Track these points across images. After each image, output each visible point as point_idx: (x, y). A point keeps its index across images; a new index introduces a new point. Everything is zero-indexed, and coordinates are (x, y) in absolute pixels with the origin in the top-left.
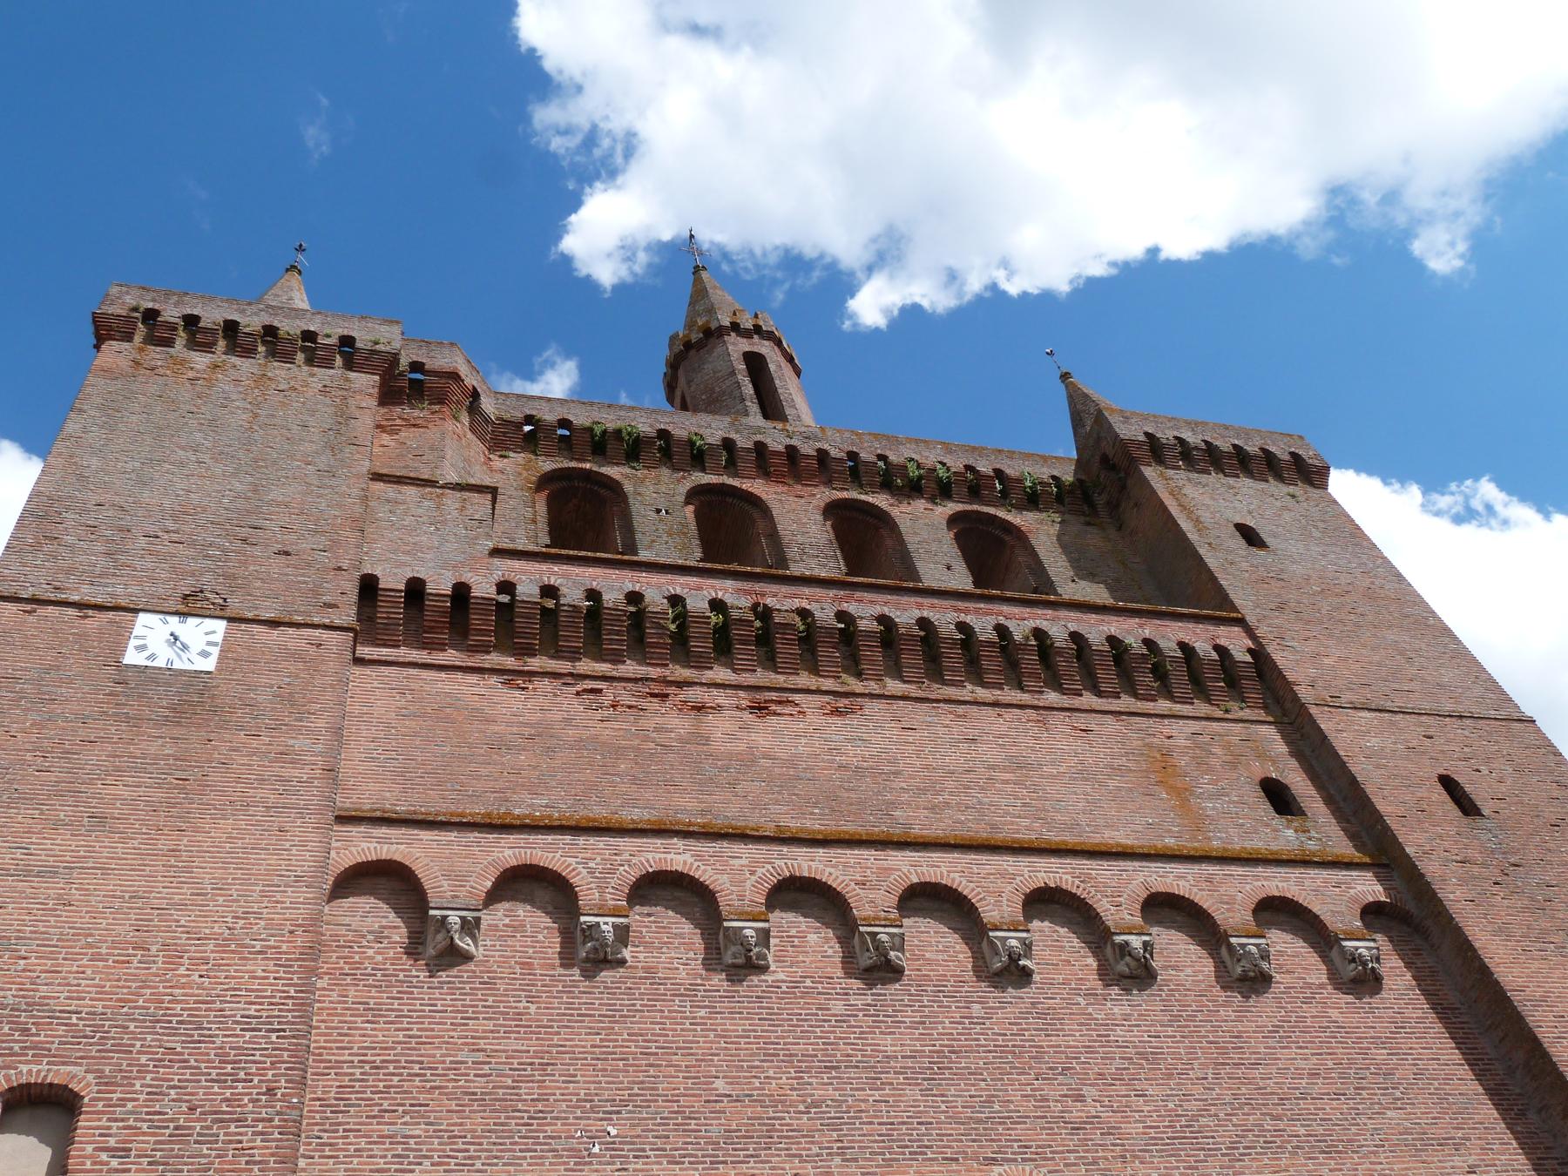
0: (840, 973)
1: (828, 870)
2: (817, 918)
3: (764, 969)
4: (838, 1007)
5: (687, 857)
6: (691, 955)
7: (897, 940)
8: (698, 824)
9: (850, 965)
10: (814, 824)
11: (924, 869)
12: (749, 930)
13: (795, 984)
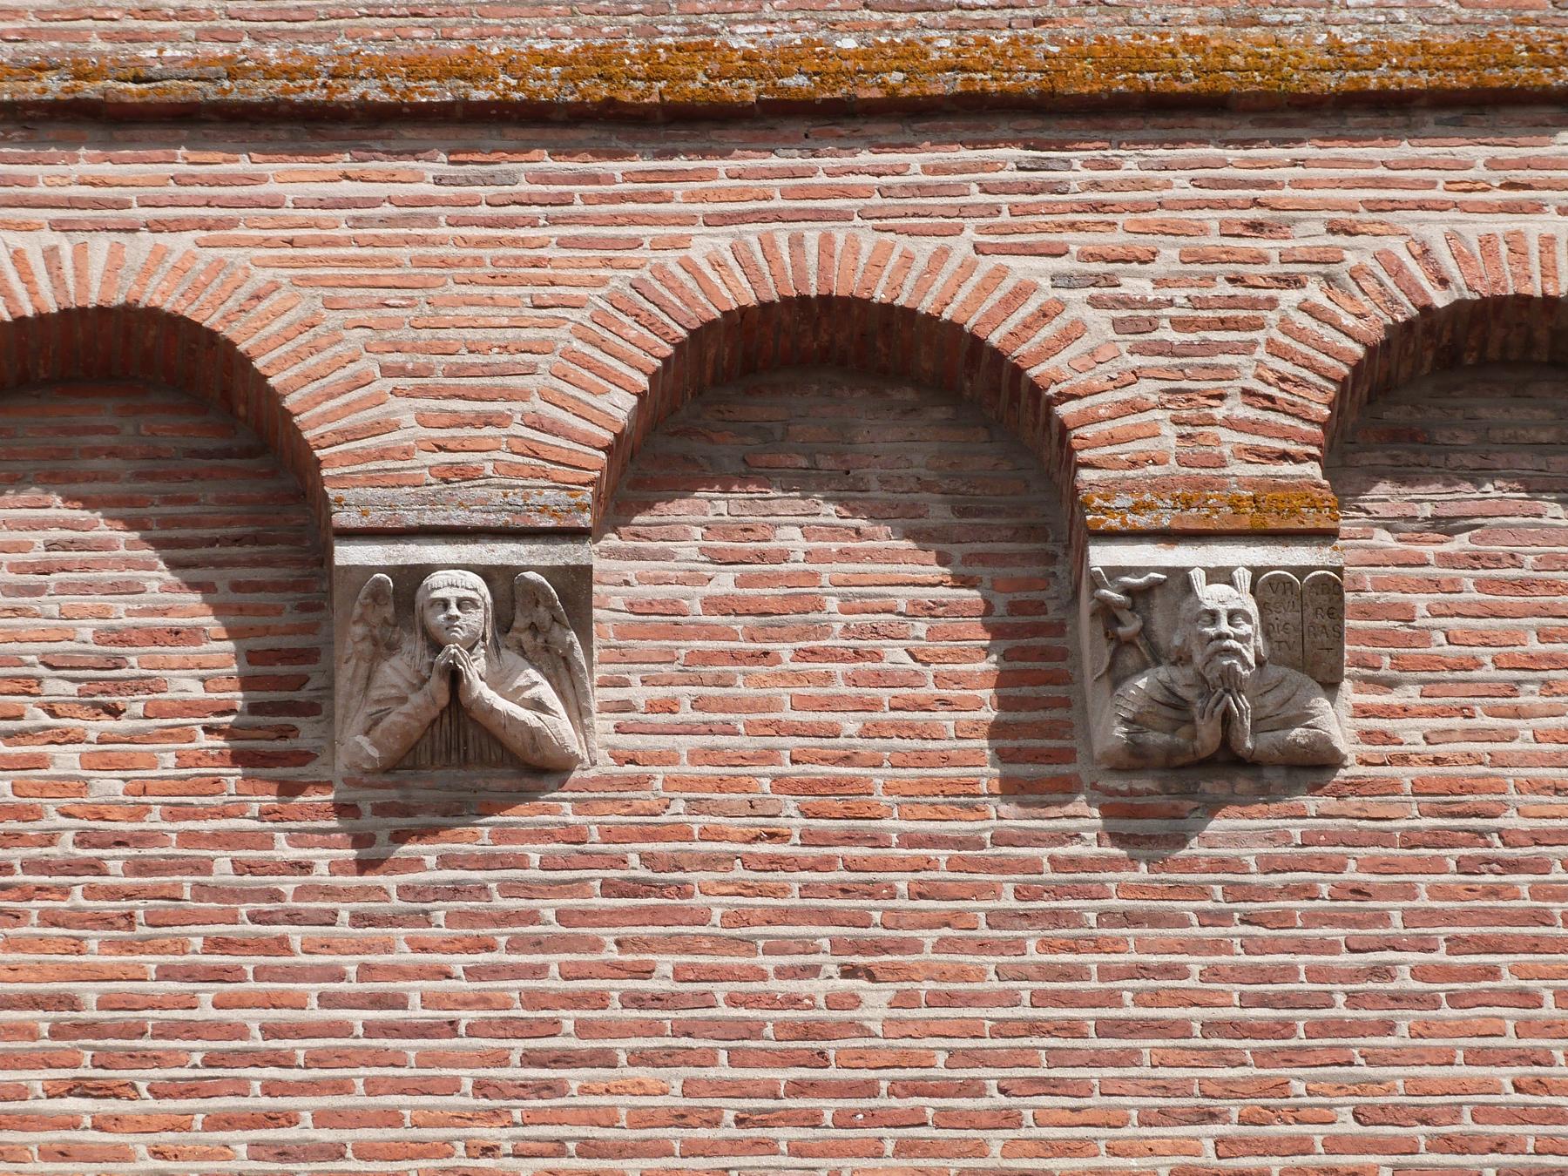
12: (1225, 582)
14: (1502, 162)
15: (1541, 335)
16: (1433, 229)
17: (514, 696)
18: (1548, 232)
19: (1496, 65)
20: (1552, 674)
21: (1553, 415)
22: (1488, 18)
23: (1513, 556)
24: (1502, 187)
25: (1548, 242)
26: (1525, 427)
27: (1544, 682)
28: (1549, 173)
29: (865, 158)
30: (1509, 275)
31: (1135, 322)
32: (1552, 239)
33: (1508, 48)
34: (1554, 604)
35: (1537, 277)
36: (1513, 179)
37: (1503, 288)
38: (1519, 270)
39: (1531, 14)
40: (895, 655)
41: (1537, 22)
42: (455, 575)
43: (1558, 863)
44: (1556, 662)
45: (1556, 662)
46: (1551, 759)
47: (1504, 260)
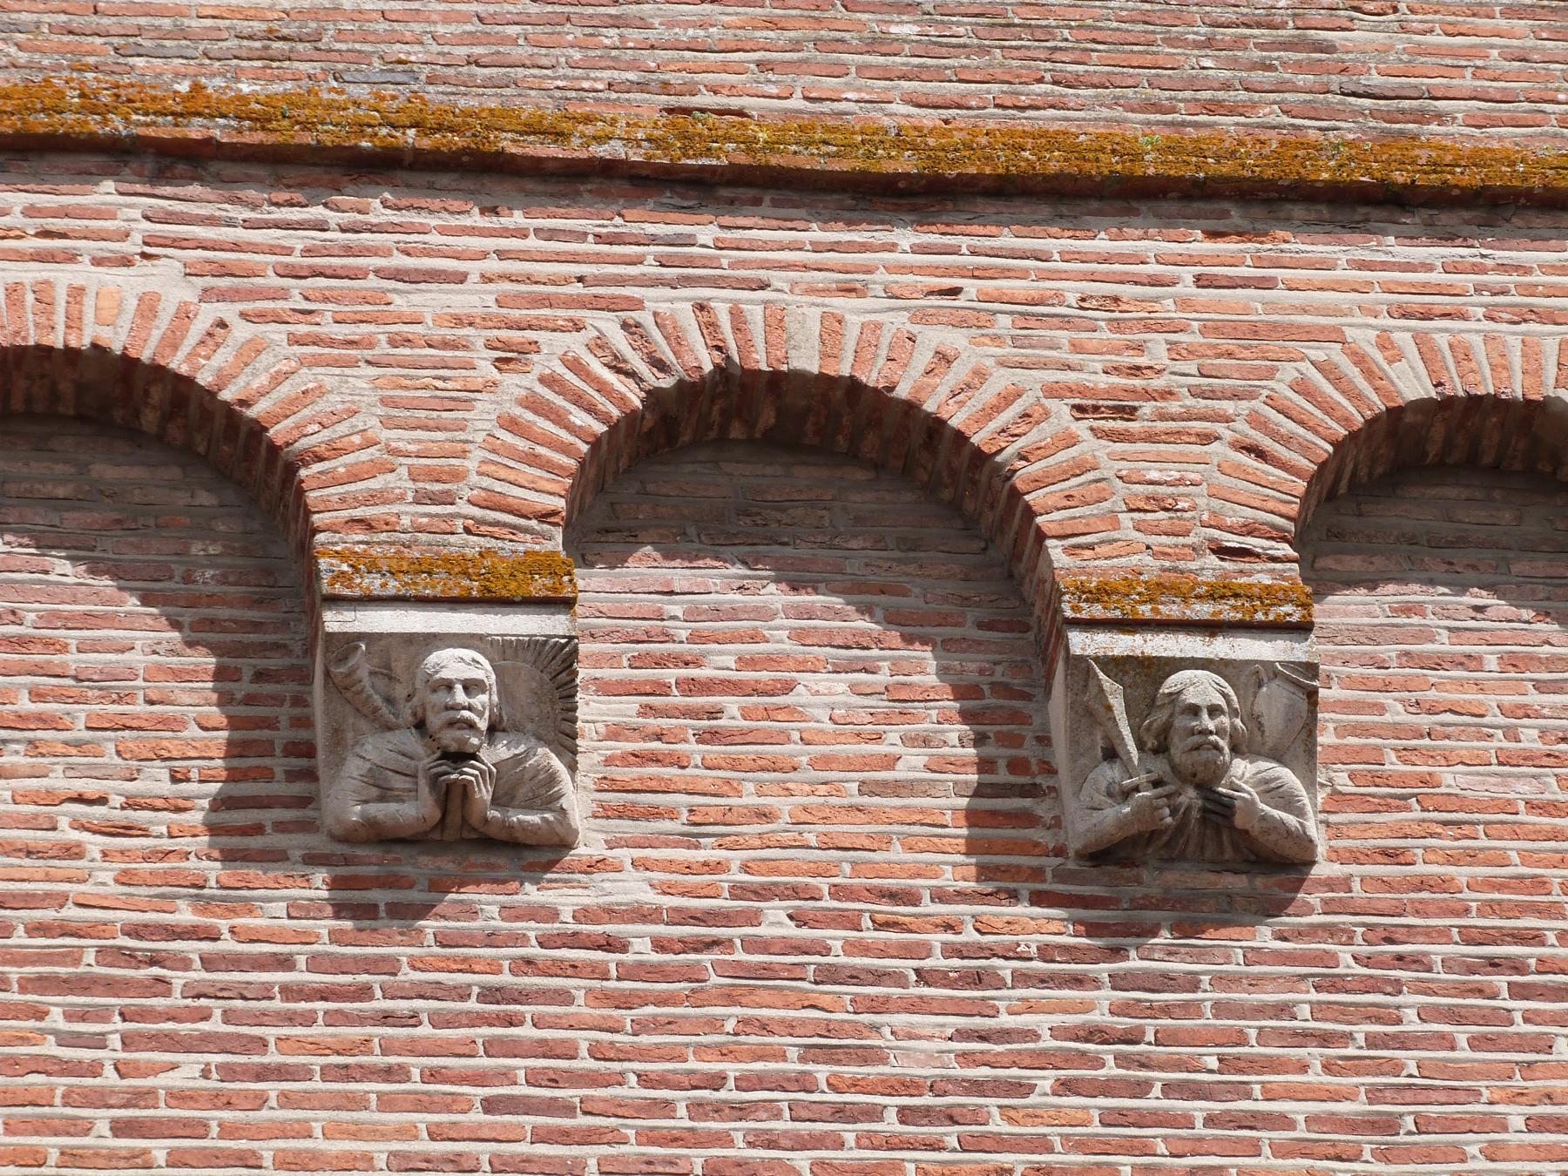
0: (955, 870)
1: (934, 337)
2: (859, 591)
3: (542, 852)
4: (923, 1045)
5: (168, 281)
6: (155, 781)
7: (1274, 702)
8: (241, 110)
9: (1009, 826)
10: (880, 102)
11: (1473, 332)
12: (462, 654)
13: (700, 930)
14: (39, 210)
15: (65, 387)
18: (77, 282)
19: (43, 110)
20: (40, 734)
21: (73, 470)
22: (46, 62)
23: (13, 613)
24: (37, 235)
25: (77, 293)
26: (42, 482)
27: (30, 742)
28: (86, 222)
29: (816, 234)
30: (31, 325)
32: (81, 290)
33: (61, 95)
34: (50, 662)
35: (61, 328)
36: (48, 227)
37: (24, 338)
38: (43, 320)
39: (91, 60)
41: (96, 68)
43: (21, 927)
44: (44, 721)
45: (44, 721)
46: (27, 821)
47: (29, 310)
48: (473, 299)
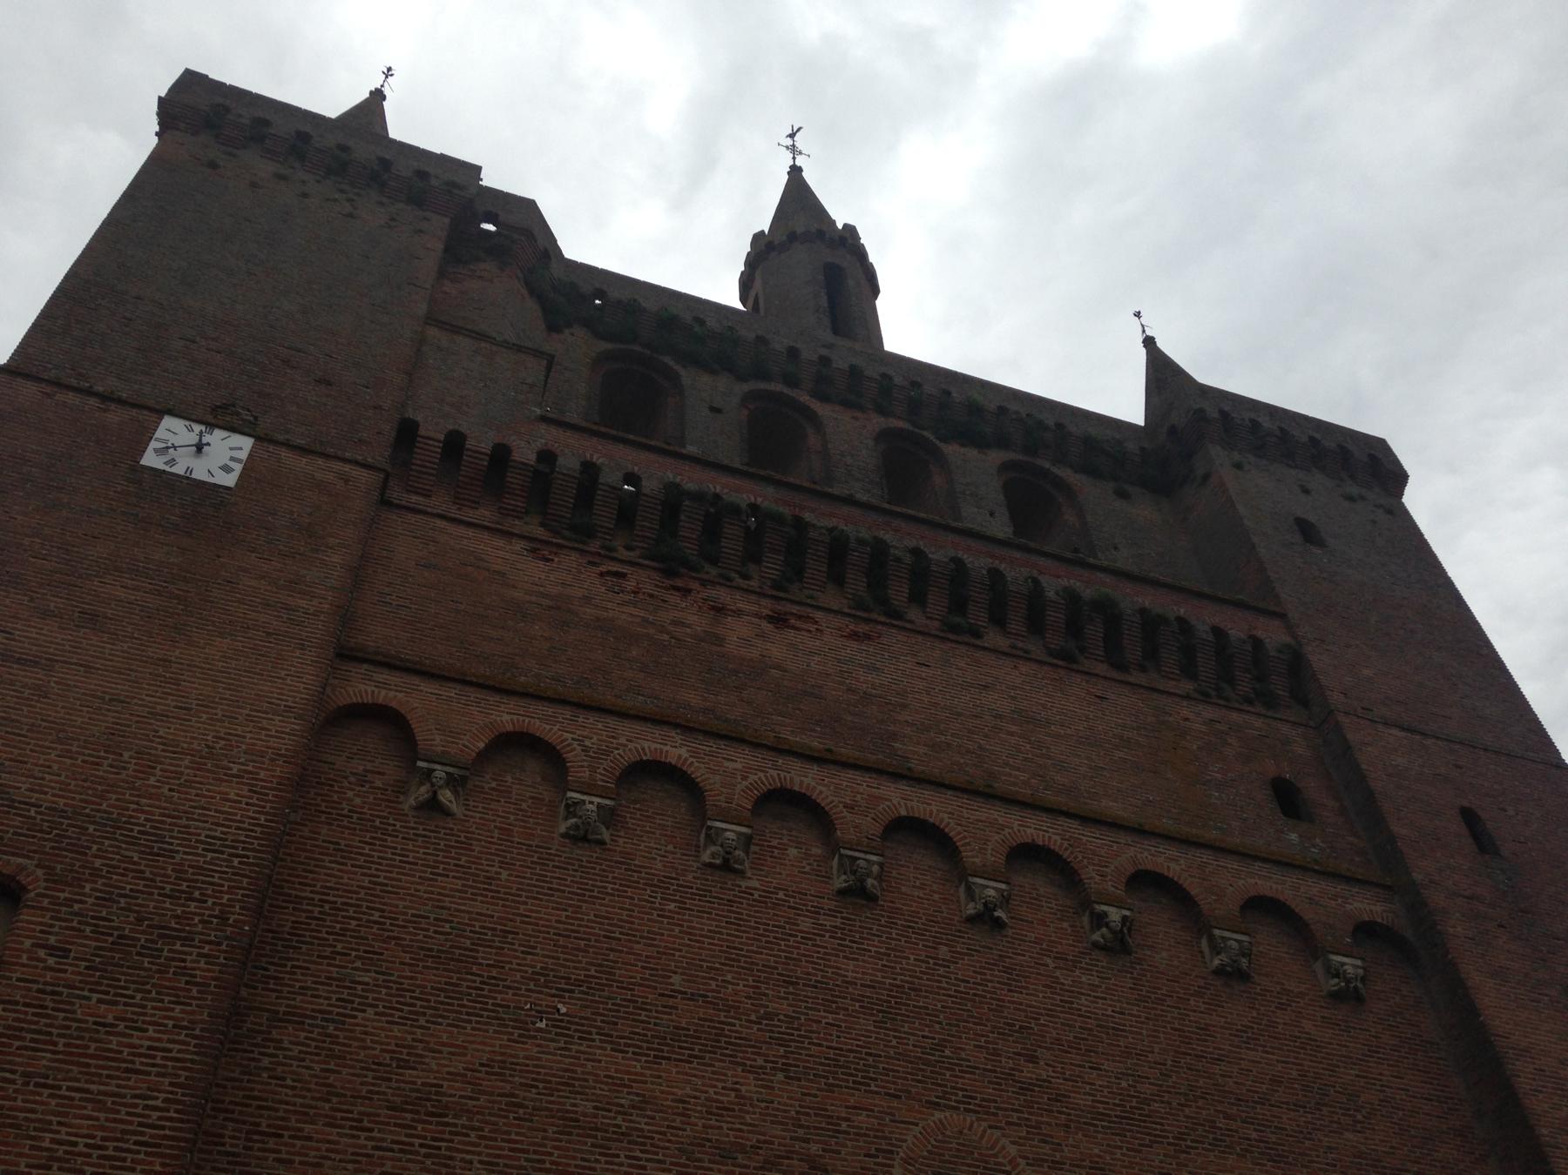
4: (806, 924)
5: (683, 752)
6: (670, 848)
16: (646, 745)
17: (446, 796)
31: (586, 750)
40: (524, 806)
42: (440, 772)
48: (739, 766)
